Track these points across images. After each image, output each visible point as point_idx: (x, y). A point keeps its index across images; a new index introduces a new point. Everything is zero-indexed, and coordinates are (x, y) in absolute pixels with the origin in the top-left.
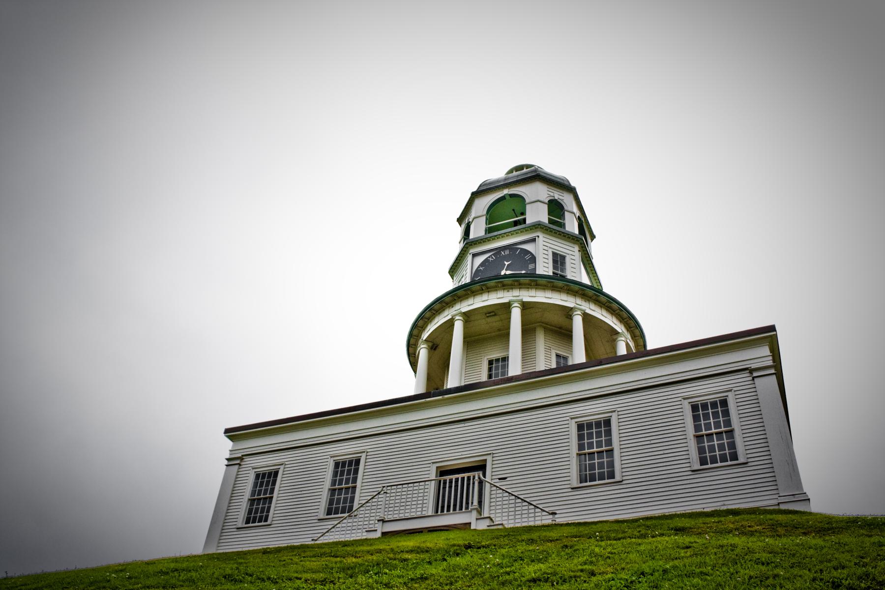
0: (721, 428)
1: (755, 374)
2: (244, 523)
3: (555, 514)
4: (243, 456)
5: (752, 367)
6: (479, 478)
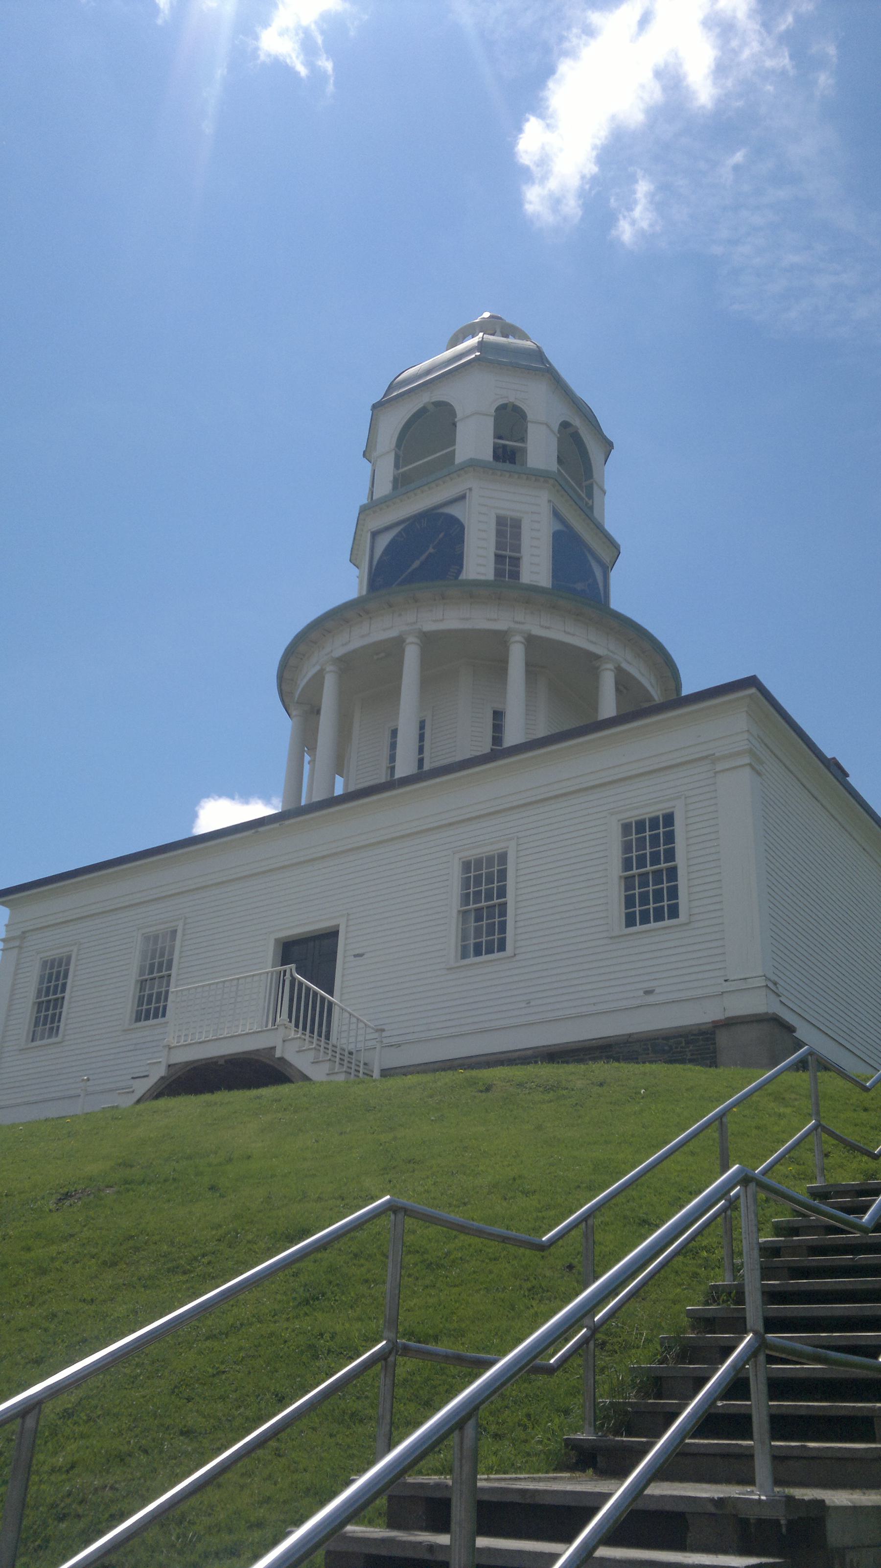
0: (660, 864)
1: (719, 767)
2: (459, 957)
3: (383, 1030)
4: (24, 933)
5: (717, 754)
6: (292, 975)
